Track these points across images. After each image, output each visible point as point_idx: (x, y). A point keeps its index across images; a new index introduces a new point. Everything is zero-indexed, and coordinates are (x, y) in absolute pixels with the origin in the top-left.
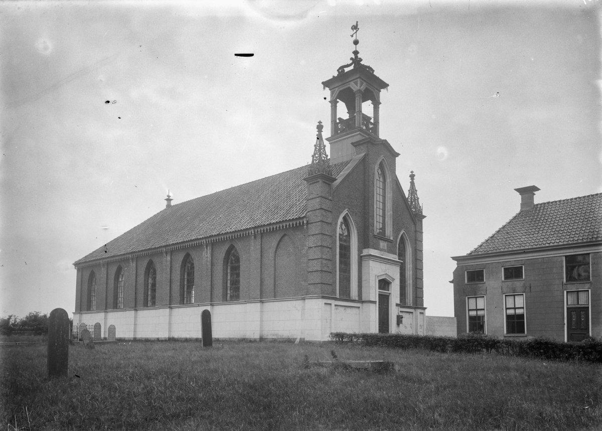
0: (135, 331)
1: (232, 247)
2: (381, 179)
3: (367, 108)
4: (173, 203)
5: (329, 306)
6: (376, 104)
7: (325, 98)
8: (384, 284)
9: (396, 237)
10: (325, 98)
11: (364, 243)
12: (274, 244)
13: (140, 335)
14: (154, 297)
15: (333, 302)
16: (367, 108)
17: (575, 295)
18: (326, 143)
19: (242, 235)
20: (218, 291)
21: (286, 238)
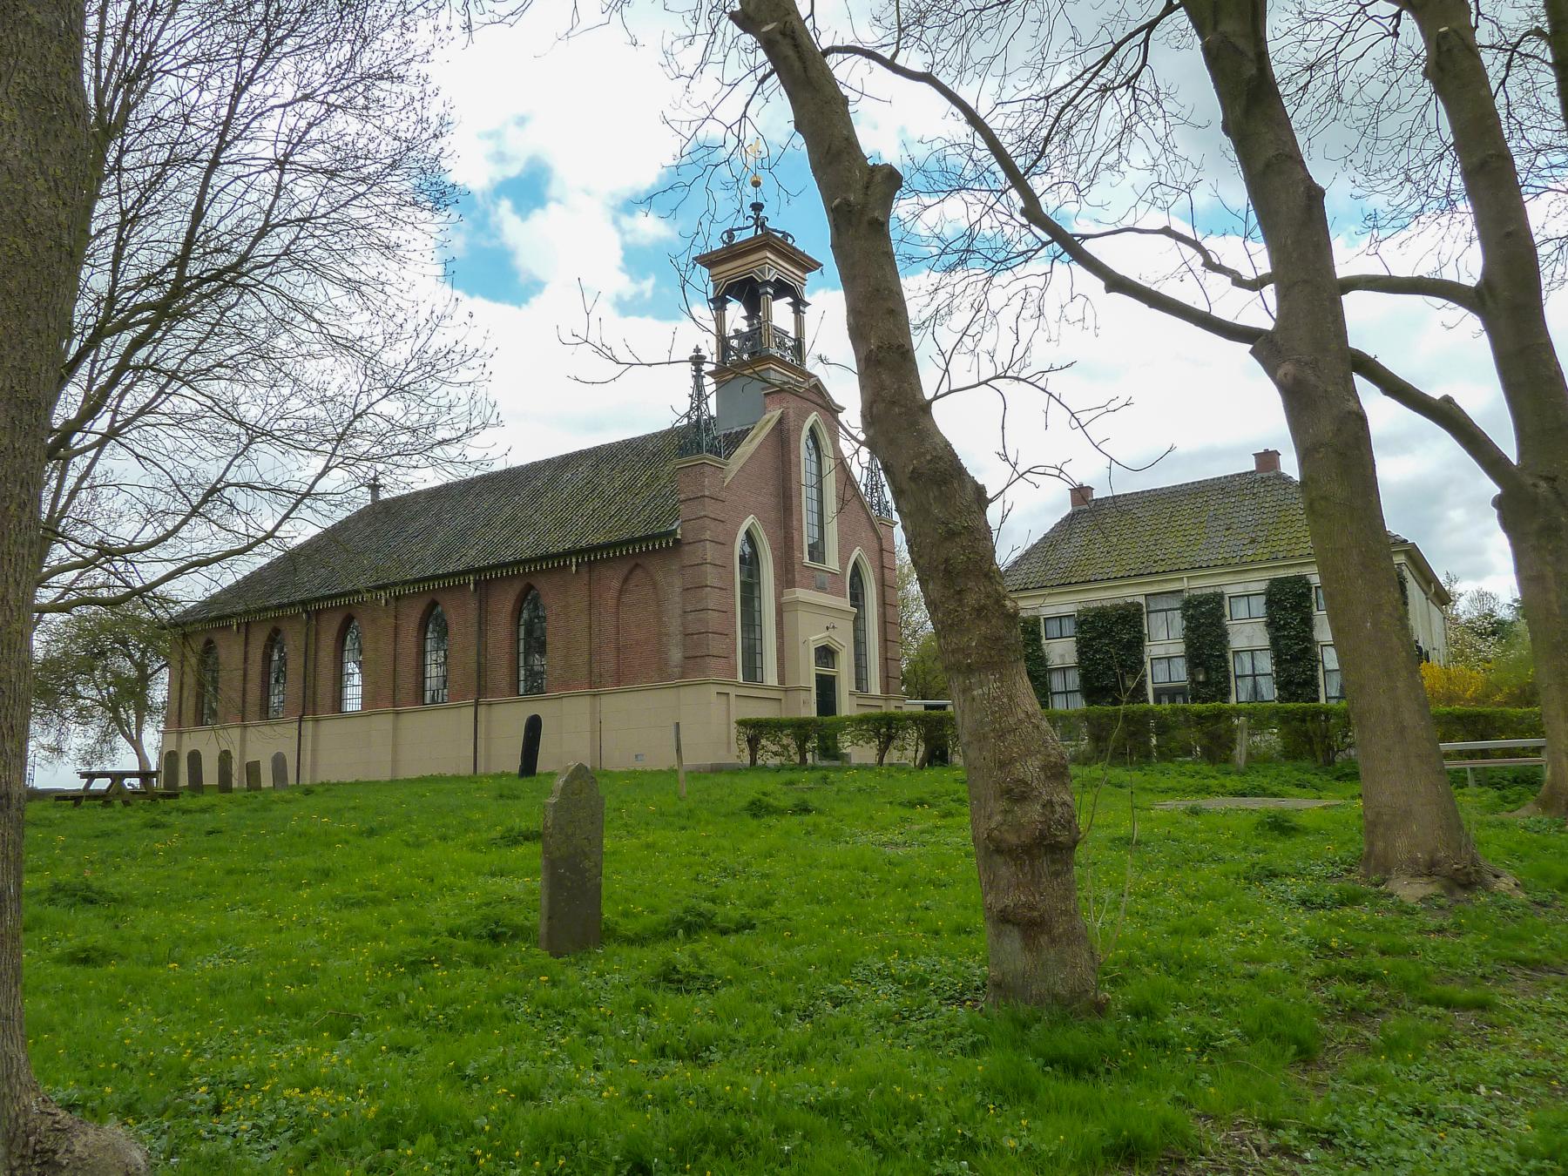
0: (395, 761)
1: (530, 587)
2: (814, 457)
3: (781, 313)
4: (384, 495)
5: (724, 697)
6: (799, 305)
7: (521, 121)
8: (826, 654)
9: (843, 565)
10: (521, 121)
11: (786, 578)
12: (616, 584)
13: (409, 772)
14: (315, 704)
15: (733, 691)
16: (781, 313)
17: (1165, 664)
18: (708, 380)
19: (552, 563)
20: (500, 674)
21: (639, 572)
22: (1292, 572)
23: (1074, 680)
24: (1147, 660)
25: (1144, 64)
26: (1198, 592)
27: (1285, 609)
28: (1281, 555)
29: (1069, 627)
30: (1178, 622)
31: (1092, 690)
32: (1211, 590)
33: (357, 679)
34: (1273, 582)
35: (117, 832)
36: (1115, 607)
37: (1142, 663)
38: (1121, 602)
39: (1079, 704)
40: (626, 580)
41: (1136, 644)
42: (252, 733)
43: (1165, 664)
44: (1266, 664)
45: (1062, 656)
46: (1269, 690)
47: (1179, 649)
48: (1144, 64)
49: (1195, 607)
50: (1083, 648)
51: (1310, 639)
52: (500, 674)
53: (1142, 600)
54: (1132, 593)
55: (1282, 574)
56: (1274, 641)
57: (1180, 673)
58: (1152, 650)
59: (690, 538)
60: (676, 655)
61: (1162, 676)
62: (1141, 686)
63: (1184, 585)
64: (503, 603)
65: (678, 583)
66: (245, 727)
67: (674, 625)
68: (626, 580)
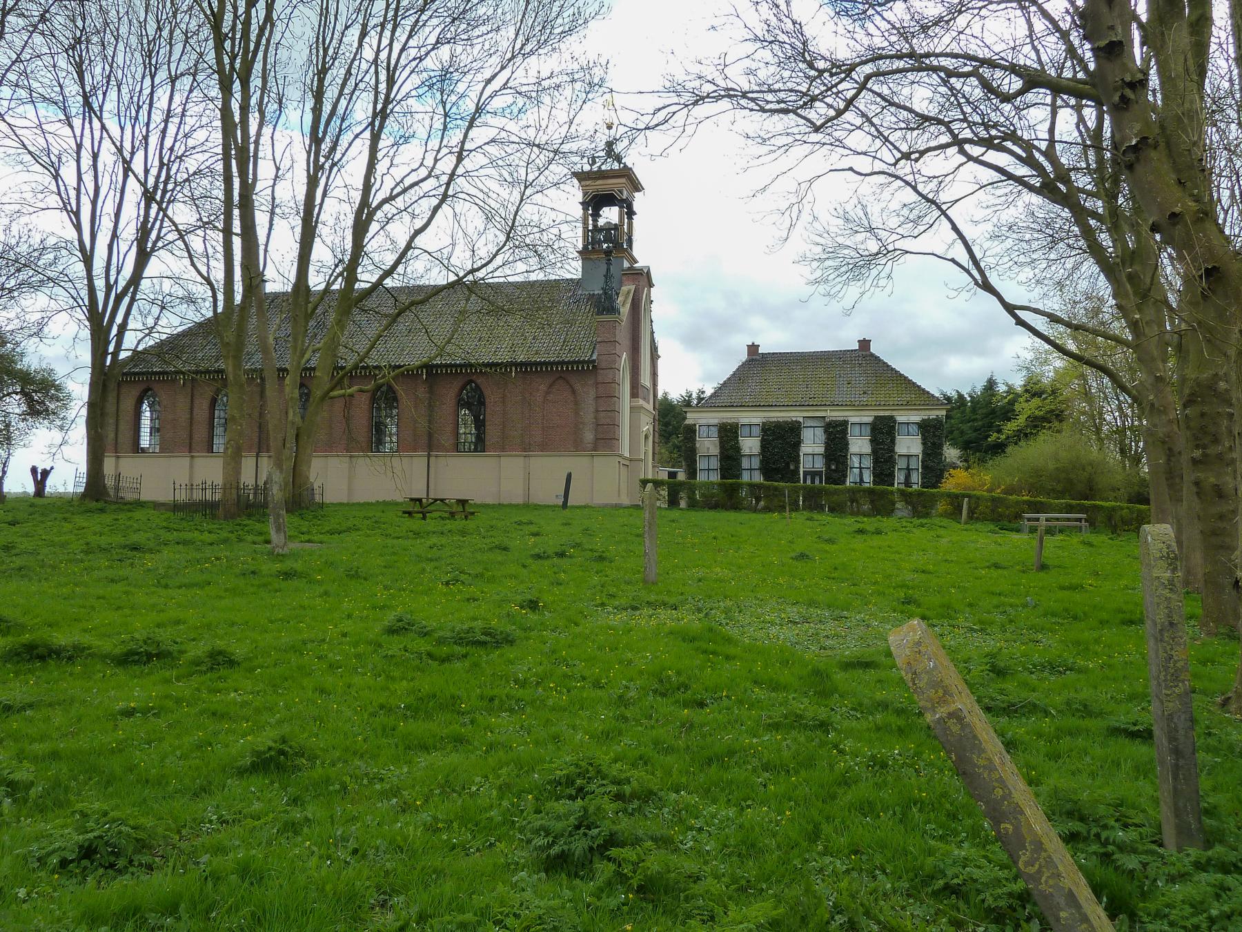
6: (631, 213)
17: (811, 457)
22: (887, 413)
23: (756, 463)
24: (801, 454)
25: (866, 175)
26: (838, 419)
27: (883, 433)
28: (883, 403)
29: (756, 431)
30: (820, 433)
31: (768, 469)
32: (842, 419)
33: (148, 414)
34: (876, 417)
35: (1062, 588)
36: (786, 422)
37: (799, 456)
38: (789, 420)
39: (758, 478)
40: (551, 386)
41: (798, 444)
42: (123, 462)
43: (811, 457)
44: (868, 462)
45: (751, 448)
46: (868, 477)
47: (821, 450)
48: (866, 175)
49: (833, 427)
50: (765, 445)
51: (893, 451)
52: (446, 439)
53: (801, 420)
54: (795, 415)
55: (882, 414)
56: (874, 451)
57: (819, 464)
58: (806, 449)
59: (603, 365)
60: (589, 436)
61: (809, 466)
62: (797, 468)
63: (828, 414)
64: (449, 393)
65: (592, 393)
66: (118, 457)
67: (588, 416)
68: (551, 386)
